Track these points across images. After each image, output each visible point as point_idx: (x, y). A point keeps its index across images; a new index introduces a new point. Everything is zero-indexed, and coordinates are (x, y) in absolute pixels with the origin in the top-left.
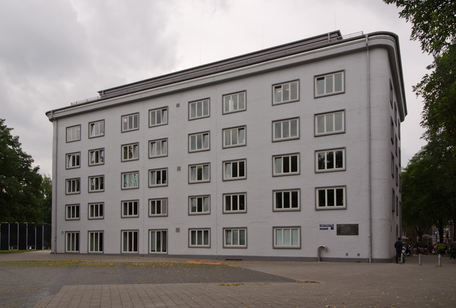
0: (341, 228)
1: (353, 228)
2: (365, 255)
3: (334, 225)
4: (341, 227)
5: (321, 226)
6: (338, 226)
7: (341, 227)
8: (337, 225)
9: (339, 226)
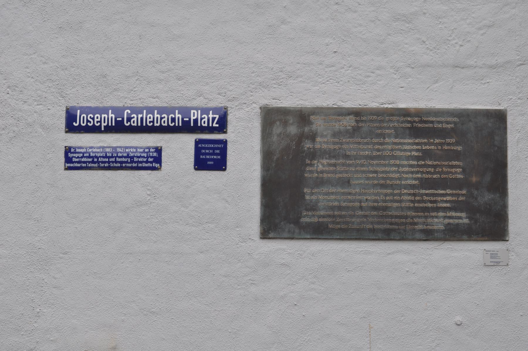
0: (313, 155)
1: (457, 156)
2: (493, 265)
3: (230, 118)
4: (313, 137)
5: (81, 120)
6: (277, 129)
7: (308, 145)
8: (224, 143)
9: (293, 130)
